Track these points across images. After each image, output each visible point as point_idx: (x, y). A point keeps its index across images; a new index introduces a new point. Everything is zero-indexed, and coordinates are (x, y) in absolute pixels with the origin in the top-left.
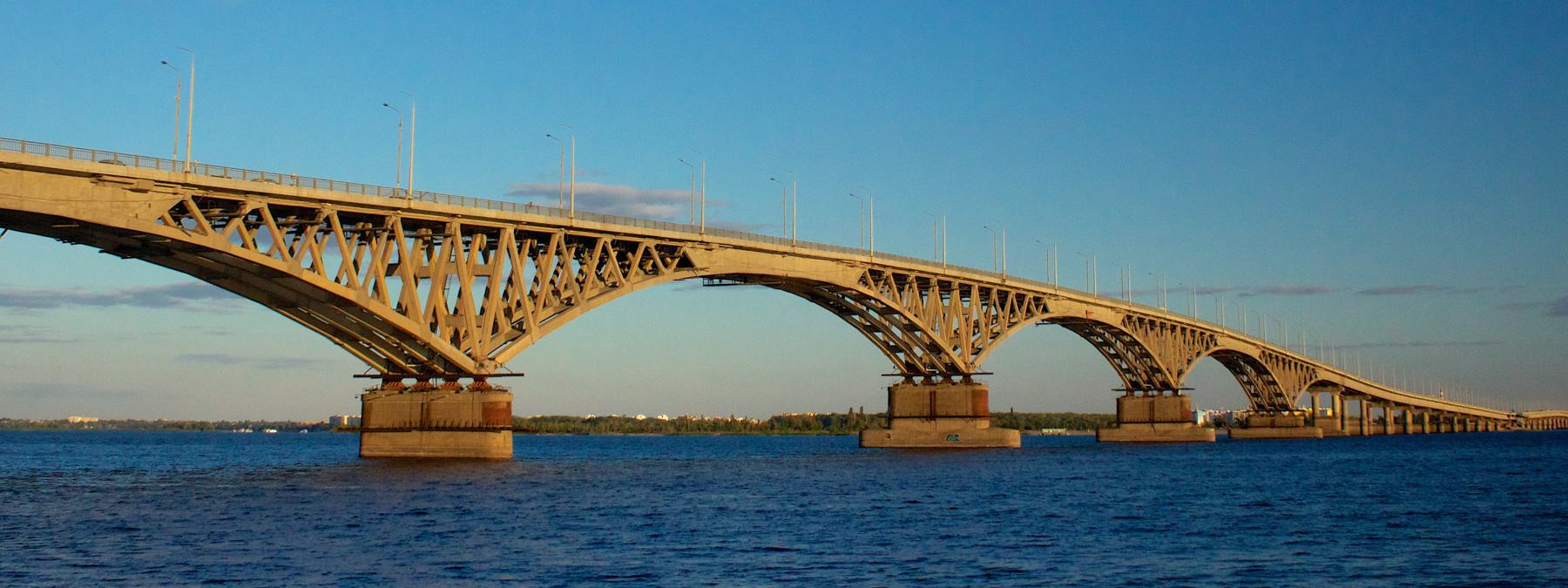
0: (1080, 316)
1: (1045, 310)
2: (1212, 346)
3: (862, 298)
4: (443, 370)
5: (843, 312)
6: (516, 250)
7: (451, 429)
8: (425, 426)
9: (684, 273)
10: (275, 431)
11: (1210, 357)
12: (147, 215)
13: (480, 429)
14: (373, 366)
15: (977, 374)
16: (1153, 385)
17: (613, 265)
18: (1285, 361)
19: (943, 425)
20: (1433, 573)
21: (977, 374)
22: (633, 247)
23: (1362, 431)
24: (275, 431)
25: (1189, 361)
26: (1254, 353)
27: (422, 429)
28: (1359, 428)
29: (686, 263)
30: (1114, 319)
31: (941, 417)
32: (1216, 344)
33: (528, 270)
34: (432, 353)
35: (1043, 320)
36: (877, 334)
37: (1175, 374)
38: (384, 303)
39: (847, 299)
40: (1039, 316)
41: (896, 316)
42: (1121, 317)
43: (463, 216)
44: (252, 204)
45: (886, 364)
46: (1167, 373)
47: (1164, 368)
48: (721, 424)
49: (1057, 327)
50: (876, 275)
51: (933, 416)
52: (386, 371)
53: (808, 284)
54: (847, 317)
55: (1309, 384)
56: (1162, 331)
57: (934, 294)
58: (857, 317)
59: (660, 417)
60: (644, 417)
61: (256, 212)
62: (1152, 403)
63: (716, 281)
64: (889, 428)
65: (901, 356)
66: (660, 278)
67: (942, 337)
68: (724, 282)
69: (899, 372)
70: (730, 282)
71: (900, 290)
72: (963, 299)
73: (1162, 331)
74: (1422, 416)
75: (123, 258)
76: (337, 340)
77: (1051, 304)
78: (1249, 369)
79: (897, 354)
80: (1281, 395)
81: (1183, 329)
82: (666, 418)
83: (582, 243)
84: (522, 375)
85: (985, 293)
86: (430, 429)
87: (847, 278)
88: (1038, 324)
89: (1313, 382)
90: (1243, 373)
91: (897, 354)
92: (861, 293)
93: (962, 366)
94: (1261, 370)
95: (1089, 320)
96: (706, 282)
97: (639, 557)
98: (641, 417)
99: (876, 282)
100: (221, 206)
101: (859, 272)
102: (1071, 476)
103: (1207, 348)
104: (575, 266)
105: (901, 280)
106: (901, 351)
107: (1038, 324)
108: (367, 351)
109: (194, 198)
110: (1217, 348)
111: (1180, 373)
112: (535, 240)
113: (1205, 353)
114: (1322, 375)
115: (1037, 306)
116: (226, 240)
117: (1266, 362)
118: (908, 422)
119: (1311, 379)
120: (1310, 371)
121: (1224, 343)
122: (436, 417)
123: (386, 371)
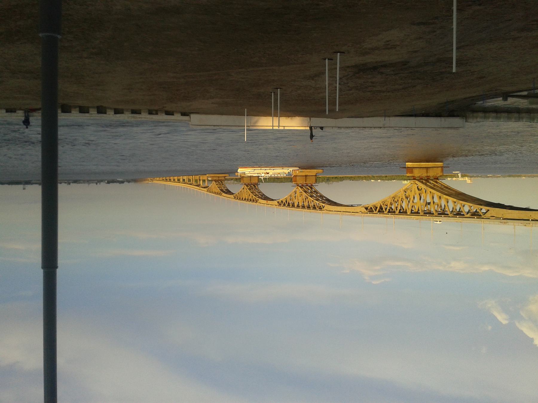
0: (269, 201)
1: (278, 202)
2: (235, 196)
3: (323, 203)
4: (423, 181)
6: (407, 210)
7: (421, 168)
8: (427, 168)
9: (367, 206)
10: (453, 172)
12: (494, 211)
13: (414, 168)
14: (441, 182)
16: (250, 186)
17: (384, 207)
18: (217, 193)
19: (304, 174)
20: (145, 130)
22: (379, 211)
23: (195, 176)
24: (453, 172)
25: (241, 192)
26: (223, 194)
27: (428, 168)
28: (195, 177)
29: (366, 208)
30: (260, 200)
31: (304, 176)
32: (234, 196)
33: (404, 205)
34: (426, 184)
36: (319, 195)
37: (245, 188)
38: (438, 195)
39: (327, 203)
40: (280, 201)
41: (315, 199)
42: (222, 195)
43: (419, 216)
44: (469, 215)
46: (247, 189)
47: (248, 190)
50: (320, 208)
51: (306, 176)
52: (437, 181)
53: (242, 165)
55: (209, 187)
56: (248, 198)
57: (306, 204)
58: (324, 199)
59: (374, 181)
60: (378, 181)
62: (250, 181)
64: (316, 173)
65: (313, 190)
66: (373, 204)
69: (314, 186)
71: (314, 206)
73: (248, 198)
74: (173, 180)
75: (499, 203)
76: (449, 187)
77: (277, 203)
78: (224, 190)
80: (217, 184)
81: (242, 199)
82: (372, 181)
83: (391, 212)
85: (293, 206)
86: (425, 168)
87: (327, 207)
89: (208, 188)
90: (226, 190)
92: (317, 201)
93: (299, 188)
94: (222, 190)
95: (266, 200)
98: (379, 181)
99: (320, 207)
100: (475, 214)
101: (324, 209)
103: (236, 195)
104: (393, 207)
105: (314, 208)
106: (314, 191)
108: (442, 185)
109: (481, 216)
110: (234, 195)
111: (244, 189)
112: (403, 212)
113: (237, 193)
114: (206, 189)
115: (280, 203)
116: (475, 208)
117: (220, 192)
118: (312, 175)
119: (208, 189)
120: (209, 190)
121: (232, 196)
122: (425, 170)
123: (437, 181)
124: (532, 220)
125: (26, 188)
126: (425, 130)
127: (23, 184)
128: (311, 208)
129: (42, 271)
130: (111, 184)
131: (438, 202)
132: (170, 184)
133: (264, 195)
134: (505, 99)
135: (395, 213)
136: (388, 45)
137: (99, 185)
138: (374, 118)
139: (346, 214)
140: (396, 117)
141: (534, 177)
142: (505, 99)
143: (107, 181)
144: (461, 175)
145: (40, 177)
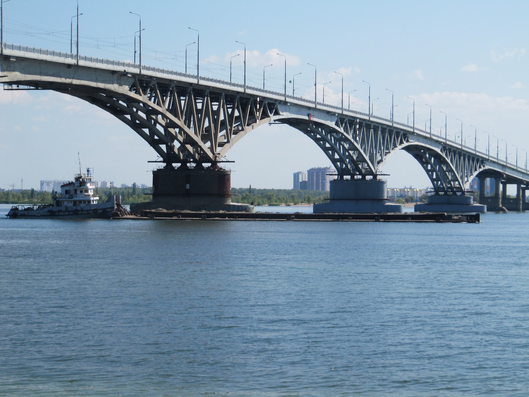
5: (118, 112)
11: (404, 151)
15: (223, 162)
21: (223, 162)
35: (275, 121)
40: (273, 117)
45: (154, 155)
48: (100, 211)
49: (286, 126)
54: (121, 116)
61: (154, 85)
63: (15, 86)
67: (196, 133)
68: (21, 87)
70: (26, 87)
72: (213, 103)
79: (330, 146)
84: (234, 162)
88: (271, 124)
91: (330, 146)
96: (6, 87)
97: (457, 288)
102: (110, 283)
107: (271, 124)
119: (480, 167)
124: (135, 63)
133: (427, 171)
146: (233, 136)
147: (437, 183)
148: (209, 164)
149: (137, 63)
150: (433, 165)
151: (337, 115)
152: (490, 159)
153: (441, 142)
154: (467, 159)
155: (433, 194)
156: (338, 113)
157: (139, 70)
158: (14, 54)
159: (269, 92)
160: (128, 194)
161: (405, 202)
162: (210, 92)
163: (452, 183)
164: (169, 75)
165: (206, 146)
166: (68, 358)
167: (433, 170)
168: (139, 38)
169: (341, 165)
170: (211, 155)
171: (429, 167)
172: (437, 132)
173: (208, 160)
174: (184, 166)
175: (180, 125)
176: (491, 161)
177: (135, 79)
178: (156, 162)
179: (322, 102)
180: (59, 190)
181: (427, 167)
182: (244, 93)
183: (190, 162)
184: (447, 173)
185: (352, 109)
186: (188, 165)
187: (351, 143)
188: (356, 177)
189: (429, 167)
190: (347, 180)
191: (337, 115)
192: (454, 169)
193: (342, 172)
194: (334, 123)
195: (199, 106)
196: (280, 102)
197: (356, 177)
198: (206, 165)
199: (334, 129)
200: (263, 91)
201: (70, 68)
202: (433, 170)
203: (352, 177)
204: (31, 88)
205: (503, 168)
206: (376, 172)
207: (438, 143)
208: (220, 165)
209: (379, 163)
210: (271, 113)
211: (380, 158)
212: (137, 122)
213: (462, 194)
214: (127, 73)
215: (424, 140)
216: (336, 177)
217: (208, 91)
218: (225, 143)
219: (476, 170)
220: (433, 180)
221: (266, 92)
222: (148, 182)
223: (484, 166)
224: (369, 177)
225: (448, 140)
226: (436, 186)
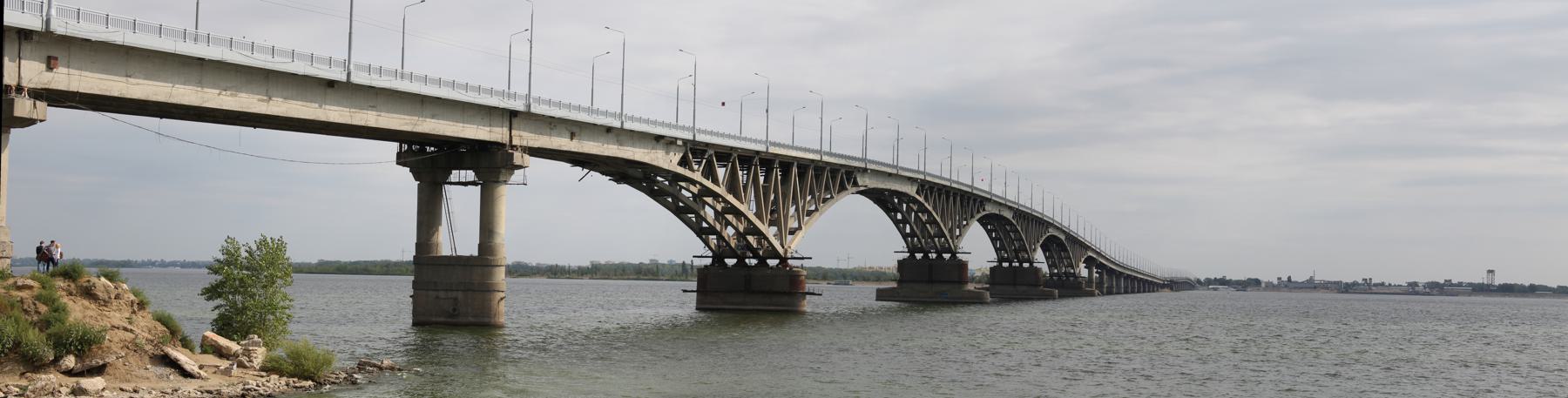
5: (657, 195)
42: (676, 157)
54: (660, 198)
61: (711, 156)
124: (196, 29)
125: (1485, 275)
126: (1442, 302)
127: (1494, 286)
128: (26, 89)
129: (638, 263)
130: (1527, 284)
131: (796, 245)
132: (1136, 275)
133: (896, 222)
134: (50, 64)
135: (879, 291)
136: (1110, 316)
137: (241, 240)
138: (574, 119)
139: (1395, 300)
140: (1309, 290)
141: (1442, 282)
142: (50, 64)
143: (960, 268)
144: (991, 294)
145: (6, 34)
146: (806, 218)
147: (912, 241)
148: (777, 261)
149: (895, 164)
150: (906, 215)
151: (680, 143)
152: (994, 198)
153: (918, 179)
154: (951, 198)
155: (708, 261)
156: (683, 139)
157: (819, 156)
158: (166, 47)
159: (750, 140)
160: (203, 340)
161: (412, 272)
162: (738, 155)
163: (230, 297)
164: (665, 129)
165: (770, 232)
166: (928, 300)
167: (905, 221)
168: (1479, 278)
169: (912, 241)
170: (781, 251)
171: (899, 216)
172: (909, 161)
173: (775, 255)
174: (926, 256)
175: (720, 193)
176: (995, 202)
177: (687, 147)
178: (702, 257)
179: (791, 144)
180: (567, 268)
181: (905, 228)
182: (767, 153)
183: (749, 258)
184: (928, 226)
185: (799, 145)
186: (747, 261)
187: (930, 214)
188: (1014, 264)
189: (899, 216)
190: (1015, 267)
191: (680, 143)
192: (938, 219)
193: (1001, 260)
194: (915, 189)
195: (934, 256)
196: (858, 169)
197: (1014, 264)
198: (773, 262)
199: (914, 198)
200: (792, 148)
201: (333, 86)
202: (905, 221)
203: (1010, 265)
204: (444, 193)
205: (39, 263)
206: (786, 251)
207: (662, 141)
208: (1035, 265)
209: (792, 232)
210: (849, 183)
211: (796, 225)
212: (681, 204)
213: (780, 263)
214: (676, 139)
215: (329, 91)
216: (995, 264)
217: (736, 155)
218: (813, 211)
219: (978, 212)
220: (905, 236)
221: (745, 139)
222: (412, 259)
223: (984, 210)
224: (1026, 265)
225: (700, 131)
226: (910, 246)
